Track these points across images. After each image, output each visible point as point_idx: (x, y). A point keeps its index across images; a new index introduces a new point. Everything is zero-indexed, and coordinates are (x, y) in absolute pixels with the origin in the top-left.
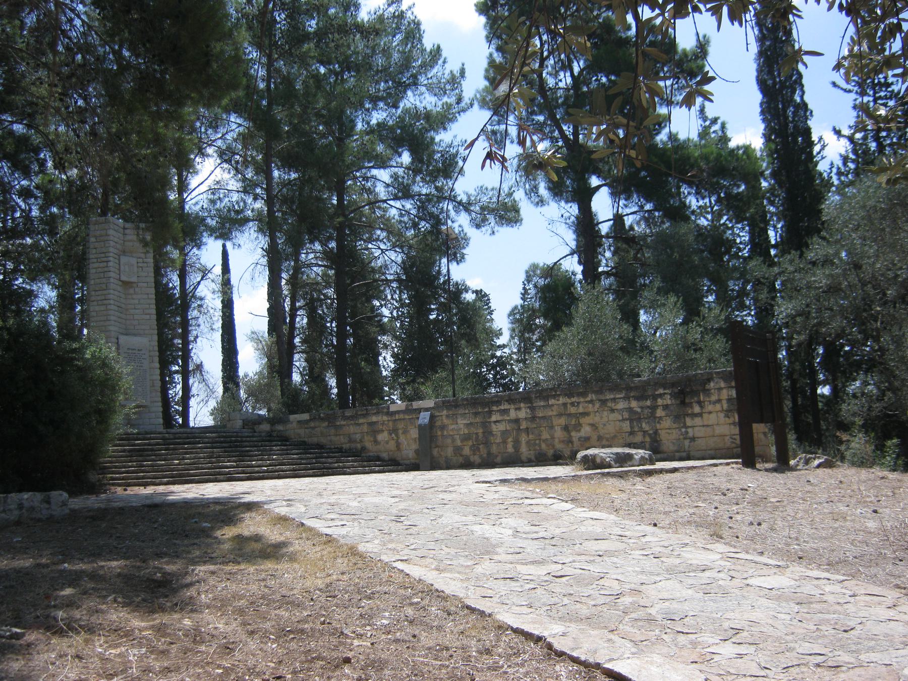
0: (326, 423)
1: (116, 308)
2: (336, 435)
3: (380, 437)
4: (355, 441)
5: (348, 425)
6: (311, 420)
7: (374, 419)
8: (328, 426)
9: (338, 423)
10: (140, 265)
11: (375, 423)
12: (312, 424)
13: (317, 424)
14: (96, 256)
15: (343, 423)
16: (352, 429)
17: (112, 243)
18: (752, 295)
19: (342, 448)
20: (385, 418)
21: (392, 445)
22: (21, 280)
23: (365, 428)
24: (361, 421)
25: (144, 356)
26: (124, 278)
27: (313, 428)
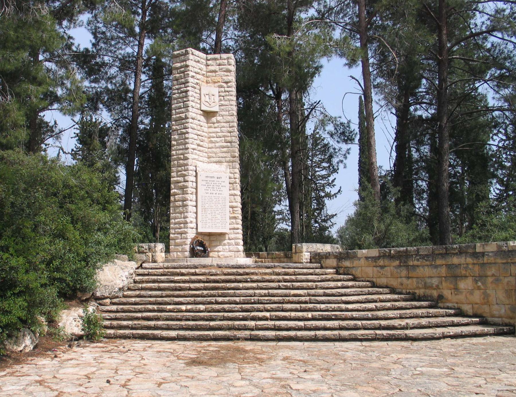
0: (397, 262)
1: (196, 137)
2: (408, 278)
3: (462, 285)
4: (431, 287)
5: (423, 266)
6: (379, 257)
7: (455, 260)
8: (400, 266)
9: (411, 263)
10: (223, 94)
11: (459, 266)
12: (381, 262)
13: (387, 262)
14: (177, 87)
15: (416, 263)
16: (427, 271)
17: (191, 74)
18: (286, 252)
19: (414, 294)
20: (469, 260)
21: (477, 296)
22: (420, 183)
23: (443, 271)
24: (439, 262)
25: (223, 184)
26: (204, 108)
27: (382, 267)
